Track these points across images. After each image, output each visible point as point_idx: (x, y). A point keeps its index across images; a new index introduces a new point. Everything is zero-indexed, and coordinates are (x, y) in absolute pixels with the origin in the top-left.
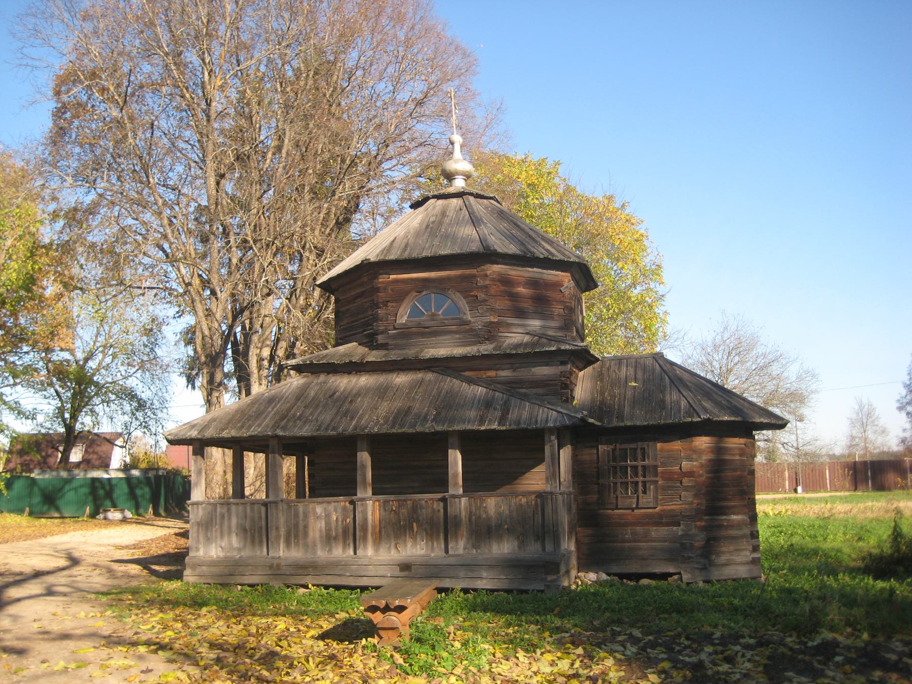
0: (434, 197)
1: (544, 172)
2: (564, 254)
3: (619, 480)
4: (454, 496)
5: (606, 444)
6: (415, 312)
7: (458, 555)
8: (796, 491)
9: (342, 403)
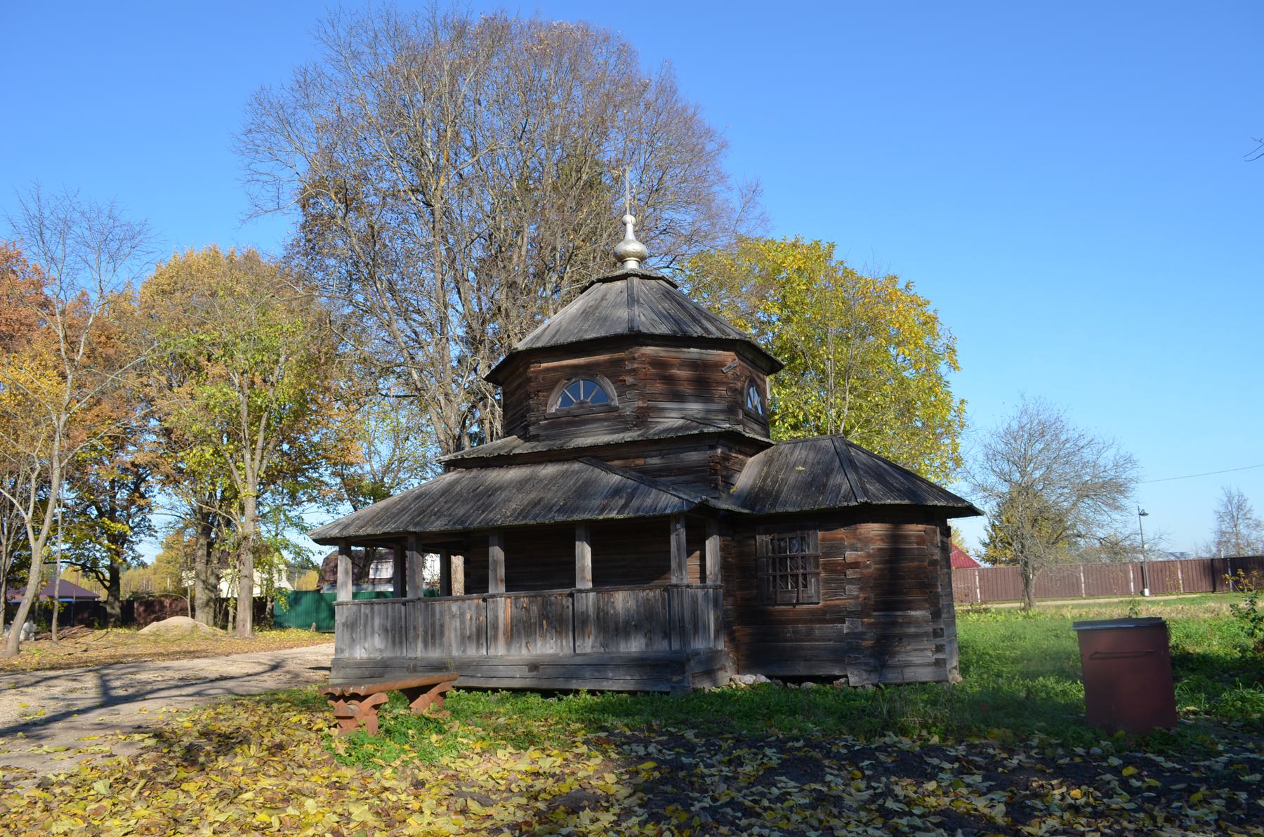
0: (599, 281)
1: (820, 254)
2: (723, 332)
3: (778, 573)
4: (580, 591)
5: (765, 533)
6: (566, 401)
8: (1142, 593)
9: (485, 496)
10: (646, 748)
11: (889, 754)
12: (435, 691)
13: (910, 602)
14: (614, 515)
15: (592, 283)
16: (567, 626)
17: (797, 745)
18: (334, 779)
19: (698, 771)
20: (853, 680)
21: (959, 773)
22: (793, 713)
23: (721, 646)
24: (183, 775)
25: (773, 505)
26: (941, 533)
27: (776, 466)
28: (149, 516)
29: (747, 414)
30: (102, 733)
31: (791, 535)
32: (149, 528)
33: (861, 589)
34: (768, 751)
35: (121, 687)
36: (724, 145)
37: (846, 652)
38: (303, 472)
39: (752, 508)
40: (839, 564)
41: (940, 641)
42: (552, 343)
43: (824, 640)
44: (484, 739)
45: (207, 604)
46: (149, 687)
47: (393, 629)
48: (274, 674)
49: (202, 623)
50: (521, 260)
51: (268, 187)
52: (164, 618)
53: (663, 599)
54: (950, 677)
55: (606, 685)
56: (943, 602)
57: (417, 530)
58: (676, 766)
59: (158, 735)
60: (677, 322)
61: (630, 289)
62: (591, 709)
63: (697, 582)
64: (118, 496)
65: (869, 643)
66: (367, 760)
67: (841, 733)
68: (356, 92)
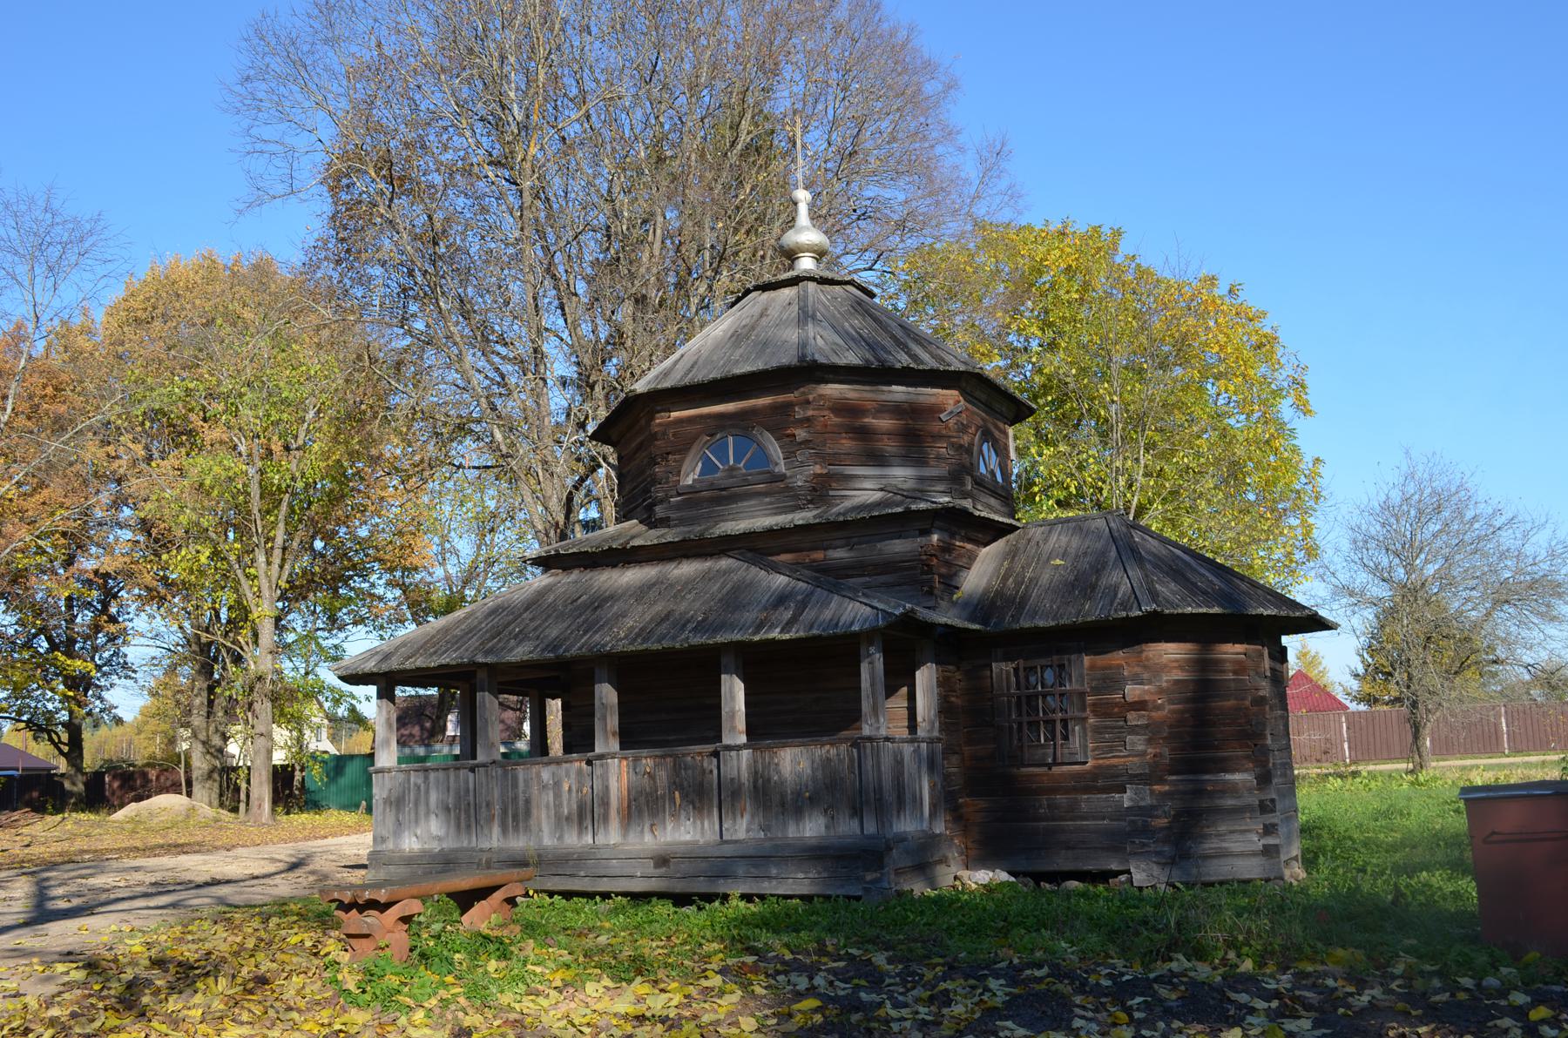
0: (757, 288)
1: (1099, 245)
3: (1025, 719)
4: (729, 748)
6: (709, 467)
7: (736, 842)
10: (811, 978)
11: (1175, 987)
12: (498, 896)
13: (1224, 759)
14: (775, 634)
15: (747, 292)
16: (711, 800)
17: (1038, 973)
18: (337, 1027)
19: (881, 1012)
20: (1139, 877)
21: (1275, 1016)
22: (1041, 925)
23: (940, 828)
24: (117, 1022)
25: (1016, 618)
26: (1271, 657)
27: (1021, 560)
28: (124, 649)
29: (979, 483)
30: (12, 963)
31: (1044, 662)
32: (125, 666)
33: (1149, 741)
34: (993, 984)
35: (62, 897)
36: (950, 86)
37: (1131, 835)
38: (346, 581)
39: (985, 622)
40: (1117, 704)
41: (1271, 819)
42: (687, 381)
43: (1095, 818)
44: (568, 966)
45: (209, 776)
46: (104, 897)
47: (457, 806)
48: (291, 875)
49: (203, 803)
50: (651, 258)
51: (277, 162)
52: (149, 797)
53: (851, 760)
54: (1287, 873)
55: (767, 887)
56: (1275, 760)
57: (489, 660)
58: (851, 1005)
59: (92, 966)
60: (872, 346)
61: (802, 299)
62: (743, 921)
63: (905, 733)
64: (79, 620)
65: (1162, 822)
66: (388, 999)
67: (1108, 956)
68: (404, 18)
